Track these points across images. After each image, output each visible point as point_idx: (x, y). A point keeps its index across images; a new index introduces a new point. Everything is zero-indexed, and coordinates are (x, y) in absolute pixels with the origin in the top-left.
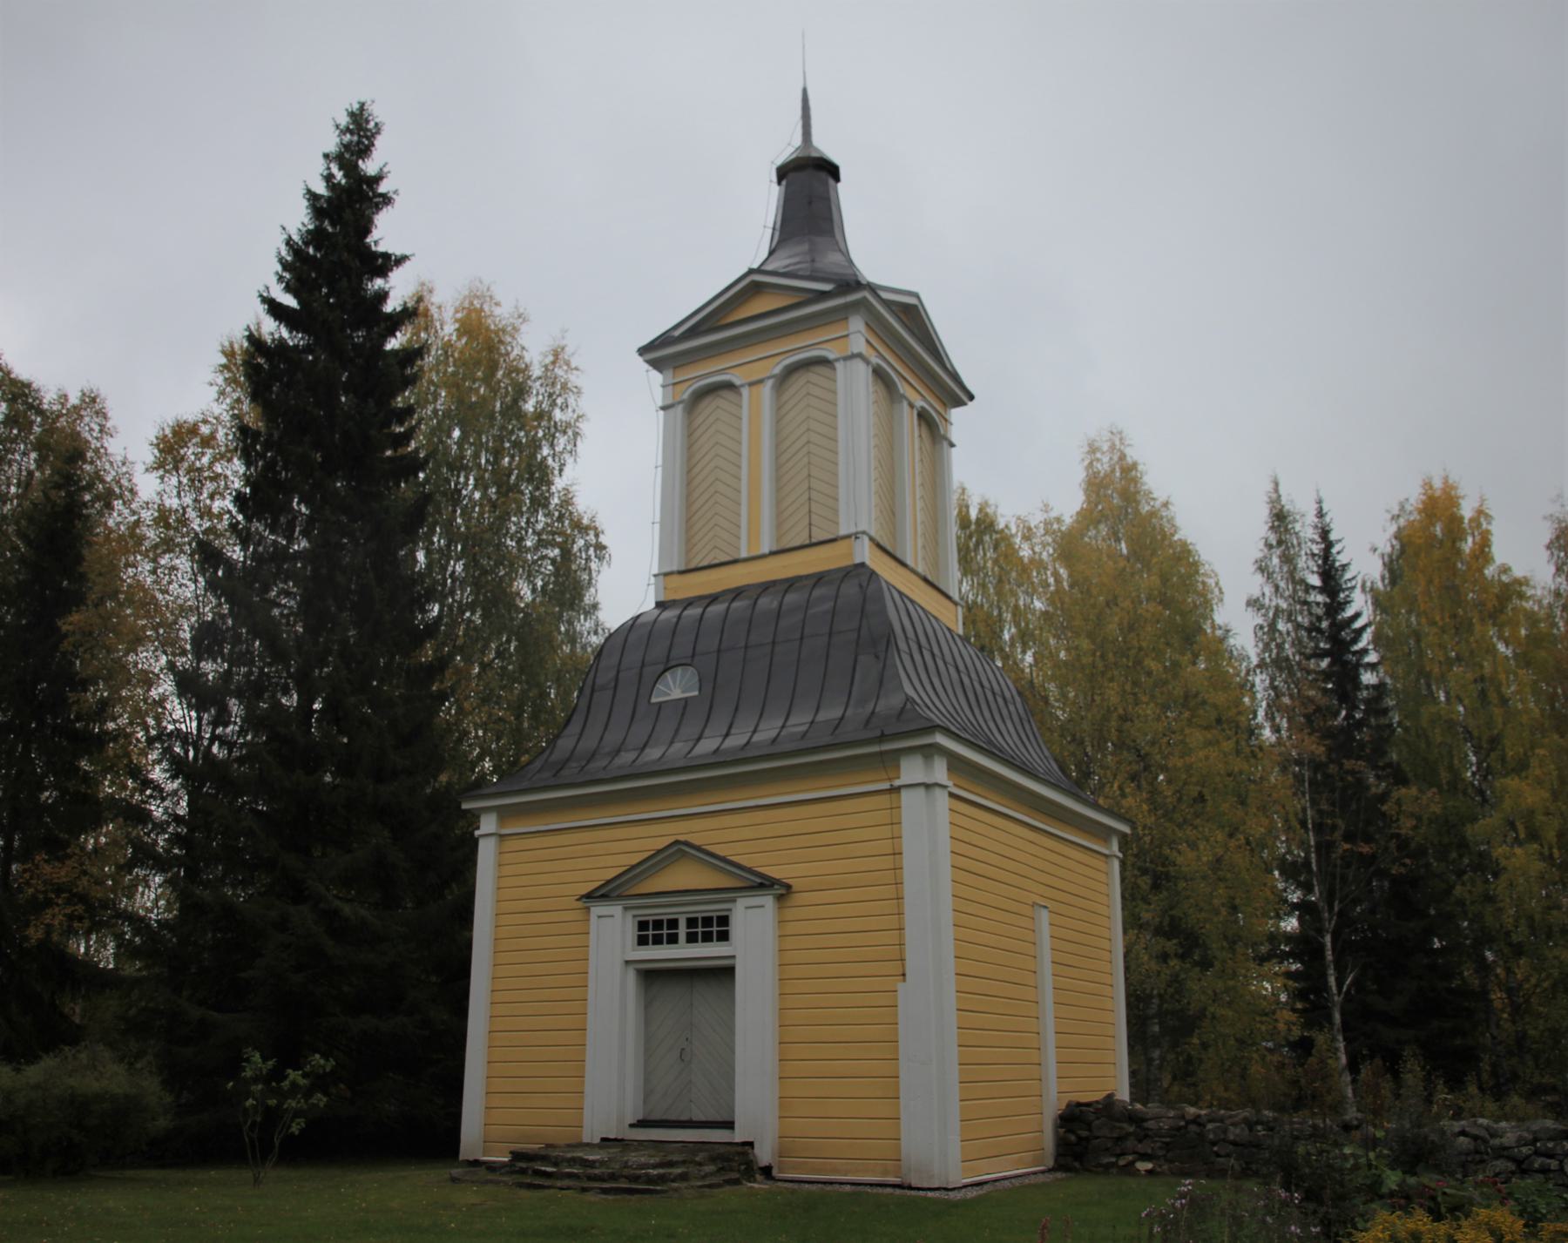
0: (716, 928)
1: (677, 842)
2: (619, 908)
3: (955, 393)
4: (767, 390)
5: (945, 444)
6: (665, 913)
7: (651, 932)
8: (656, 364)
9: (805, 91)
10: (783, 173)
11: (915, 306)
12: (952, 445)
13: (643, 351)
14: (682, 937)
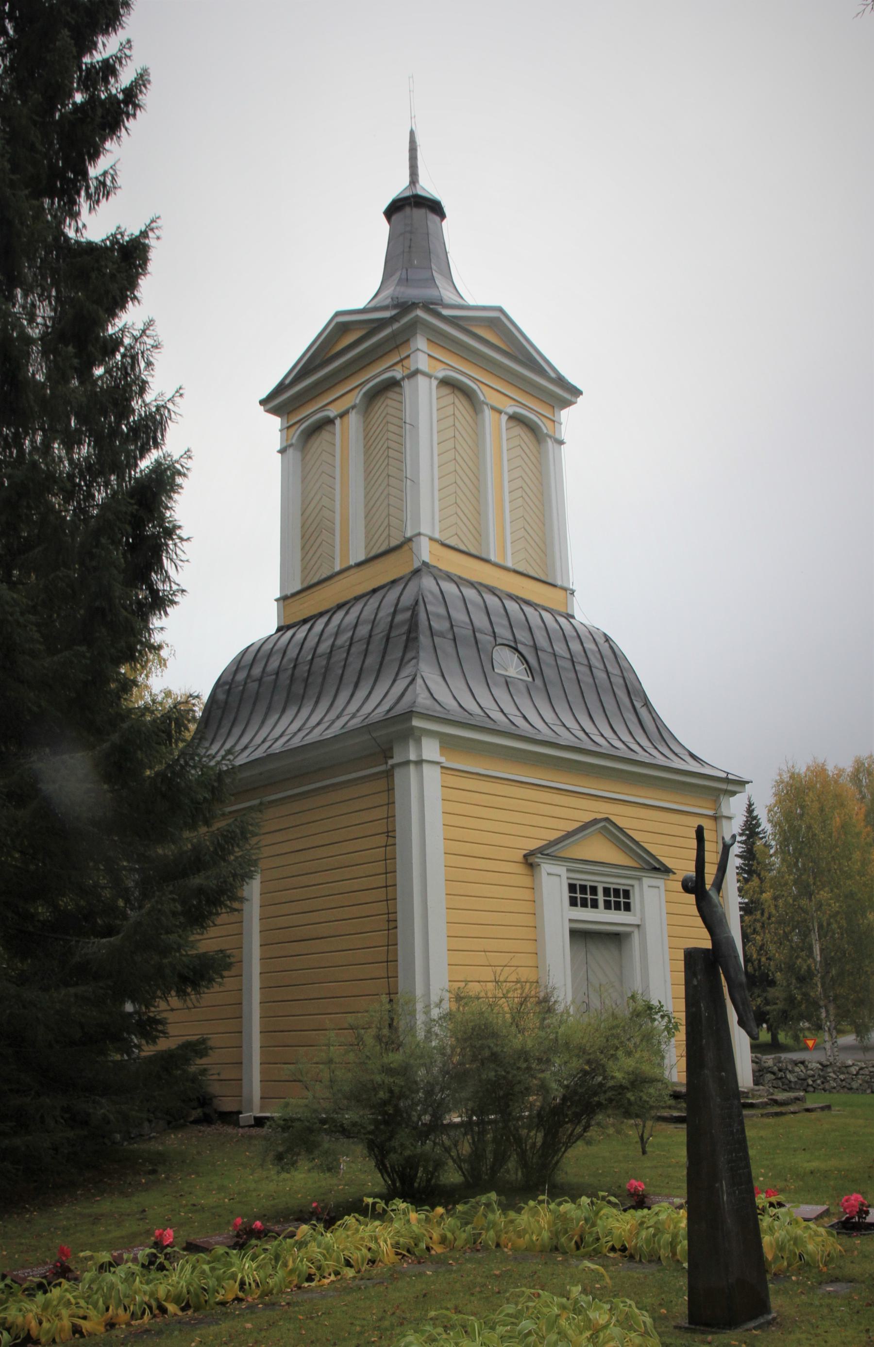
0: (620, 899)
1: (607, 820)
2: (565, 869)
3: (564, 393)
4: (353, 418)
5: (550, 442)
6: (588, 880)
7: (581, 896)
8: (275, 411)
9: (412, 133)
10: (393, 210)
11: (498, 319)
12: (561, 443)
13: (263, 402)
14: (601, 904)
